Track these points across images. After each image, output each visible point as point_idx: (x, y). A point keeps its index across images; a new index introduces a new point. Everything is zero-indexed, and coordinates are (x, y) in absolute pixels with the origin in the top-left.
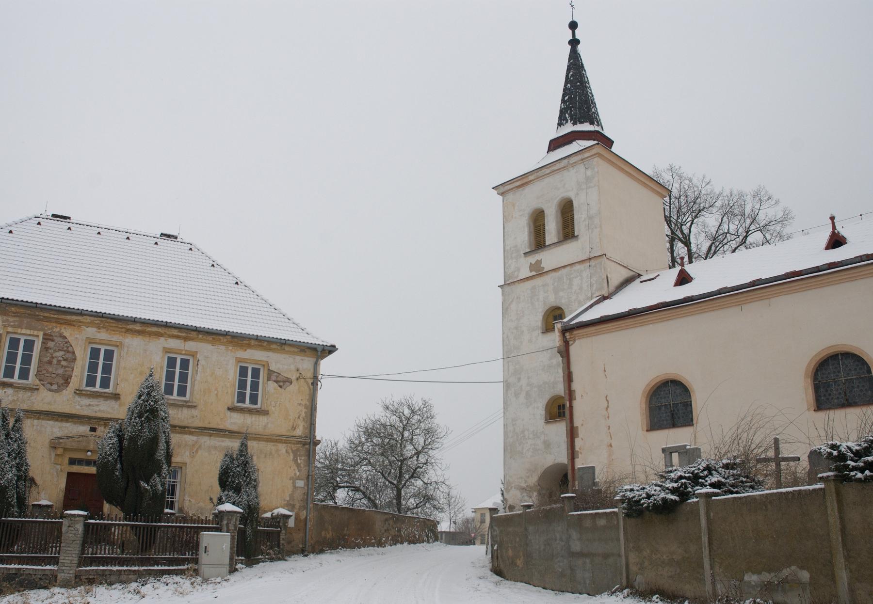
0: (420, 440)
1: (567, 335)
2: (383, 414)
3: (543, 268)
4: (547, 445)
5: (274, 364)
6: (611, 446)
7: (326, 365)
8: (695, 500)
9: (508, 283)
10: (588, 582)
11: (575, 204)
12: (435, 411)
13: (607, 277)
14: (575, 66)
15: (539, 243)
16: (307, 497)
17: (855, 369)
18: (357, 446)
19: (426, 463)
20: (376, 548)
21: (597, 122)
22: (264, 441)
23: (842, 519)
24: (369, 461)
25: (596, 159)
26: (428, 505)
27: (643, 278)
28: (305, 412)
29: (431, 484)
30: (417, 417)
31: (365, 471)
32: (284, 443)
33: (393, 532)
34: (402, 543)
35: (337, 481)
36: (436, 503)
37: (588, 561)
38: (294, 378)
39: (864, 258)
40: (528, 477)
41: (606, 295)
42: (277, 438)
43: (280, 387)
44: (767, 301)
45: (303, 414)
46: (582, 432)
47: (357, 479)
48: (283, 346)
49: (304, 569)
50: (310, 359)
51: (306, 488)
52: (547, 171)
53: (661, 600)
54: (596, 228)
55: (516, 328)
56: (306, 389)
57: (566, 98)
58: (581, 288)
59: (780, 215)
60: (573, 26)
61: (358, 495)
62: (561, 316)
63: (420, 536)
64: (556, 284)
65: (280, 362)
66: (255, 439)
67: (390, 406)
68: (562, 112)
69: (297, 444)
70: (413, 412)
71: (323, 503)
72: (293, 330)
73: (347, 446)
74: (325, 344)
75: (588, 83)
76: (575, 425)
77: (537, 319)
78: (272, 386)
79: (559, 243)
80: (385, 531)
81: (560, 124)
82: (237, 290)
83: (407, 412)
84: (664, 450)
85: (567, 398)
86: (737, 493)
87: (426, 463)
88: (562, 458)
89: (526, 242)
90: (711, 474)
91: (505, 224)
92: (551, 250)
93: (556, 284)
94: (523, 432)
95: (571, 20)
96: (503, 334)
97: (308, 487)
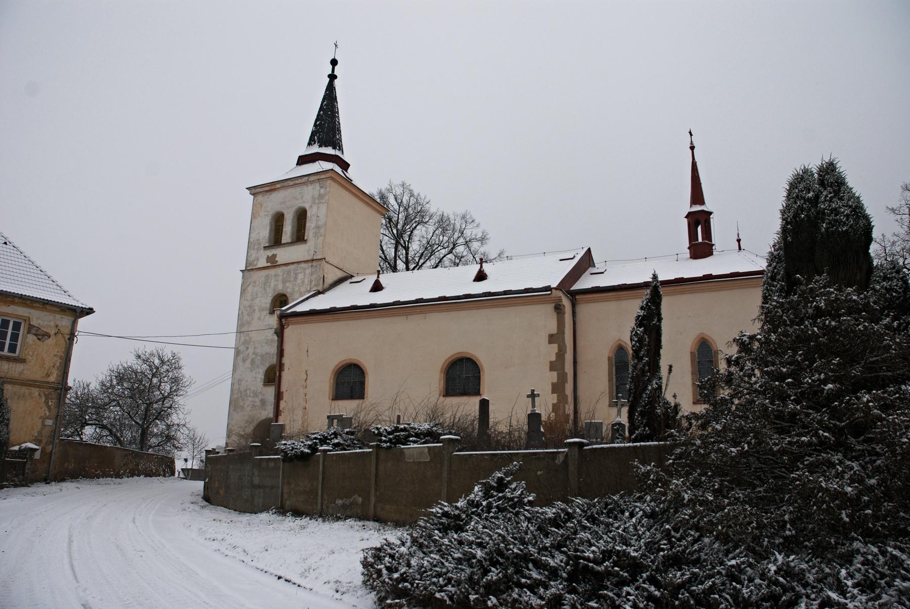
0: (166, 387)
1: (283, 320)
2: (135, 362)
3: (277, 261)
4: (263, 402)
5: (35, 319)
6: (305, 408)
7: (83, 323)
8: (319, 453)
9: (248, 268)
10: (260, 505)
11: (309, 214)
12: (182, 363)
13: (324, 277)
14: (330, 96)
15: (276, 240)
16: (55, 433)
17: (472, 370)
18: (109, 388)
19: (170, 407)
20: (114, 479)
21: (340, 148)
22: (18, 385)
23: (377, 469)
24: (118, 403)
25: (329, 181)
26: (168, 444)
27: (354, 280)
28: (60, 363)
29: (173, 425)
30: (165, 367)
31: (115, 411)
32: (38, 387)
33: (131, 466)
34: (139, 475)
35: (86, 419)
36: (176, 443)
37: (262, 491)
38: (52, 332)
39: (487, 294)
40: (246, 427)
41: (321, 291)
42: (32, 383)
43: (39, 339)
44: (424, 315)
45: (58, 364)
46: (286, 396)
47: (105, 418)
48: (46, 305)
49: (45, 493)
50: (69, 318)
51: (54, 426)
52: (291, 183)
53: (292, 515)
54: (321, 236)
55: (250, 307)
56: (63, 343)
57: (318, 123)
58: (303, 282)
59: (479, 235)
60: (334, 62)
61: (105, 433)
62: (285, 302)
63: (157, 470)
64: (285, 276)
65: (39, 318)
66: (10, 383)
67: (142, 356)
68: (313, 134)
69: (50, 389)
70: (163, 362)
71: (70, 438)
72: (56, 291)
73: (98, 387)
74: (84, 306)
75: (338, 114)
76: (281, 391)
77: (267, 301)
78: (31, 338)
79: (292, 243)
80: (124, 465)
81: (309, 144)
82: (5, 249)
83: (157, 362)
84: (328, 417)
85: (278, 368)
86: (349, 450)
87: (170, 407)
88: (269, 412)
89: (267, 238)
90: (337, 438)
91: (253, 221)
92: (285, 248)
93: (285, 276)
94: (246, 391)
95: (333, 58)
96: (239, 309)
97: (56, 426)
